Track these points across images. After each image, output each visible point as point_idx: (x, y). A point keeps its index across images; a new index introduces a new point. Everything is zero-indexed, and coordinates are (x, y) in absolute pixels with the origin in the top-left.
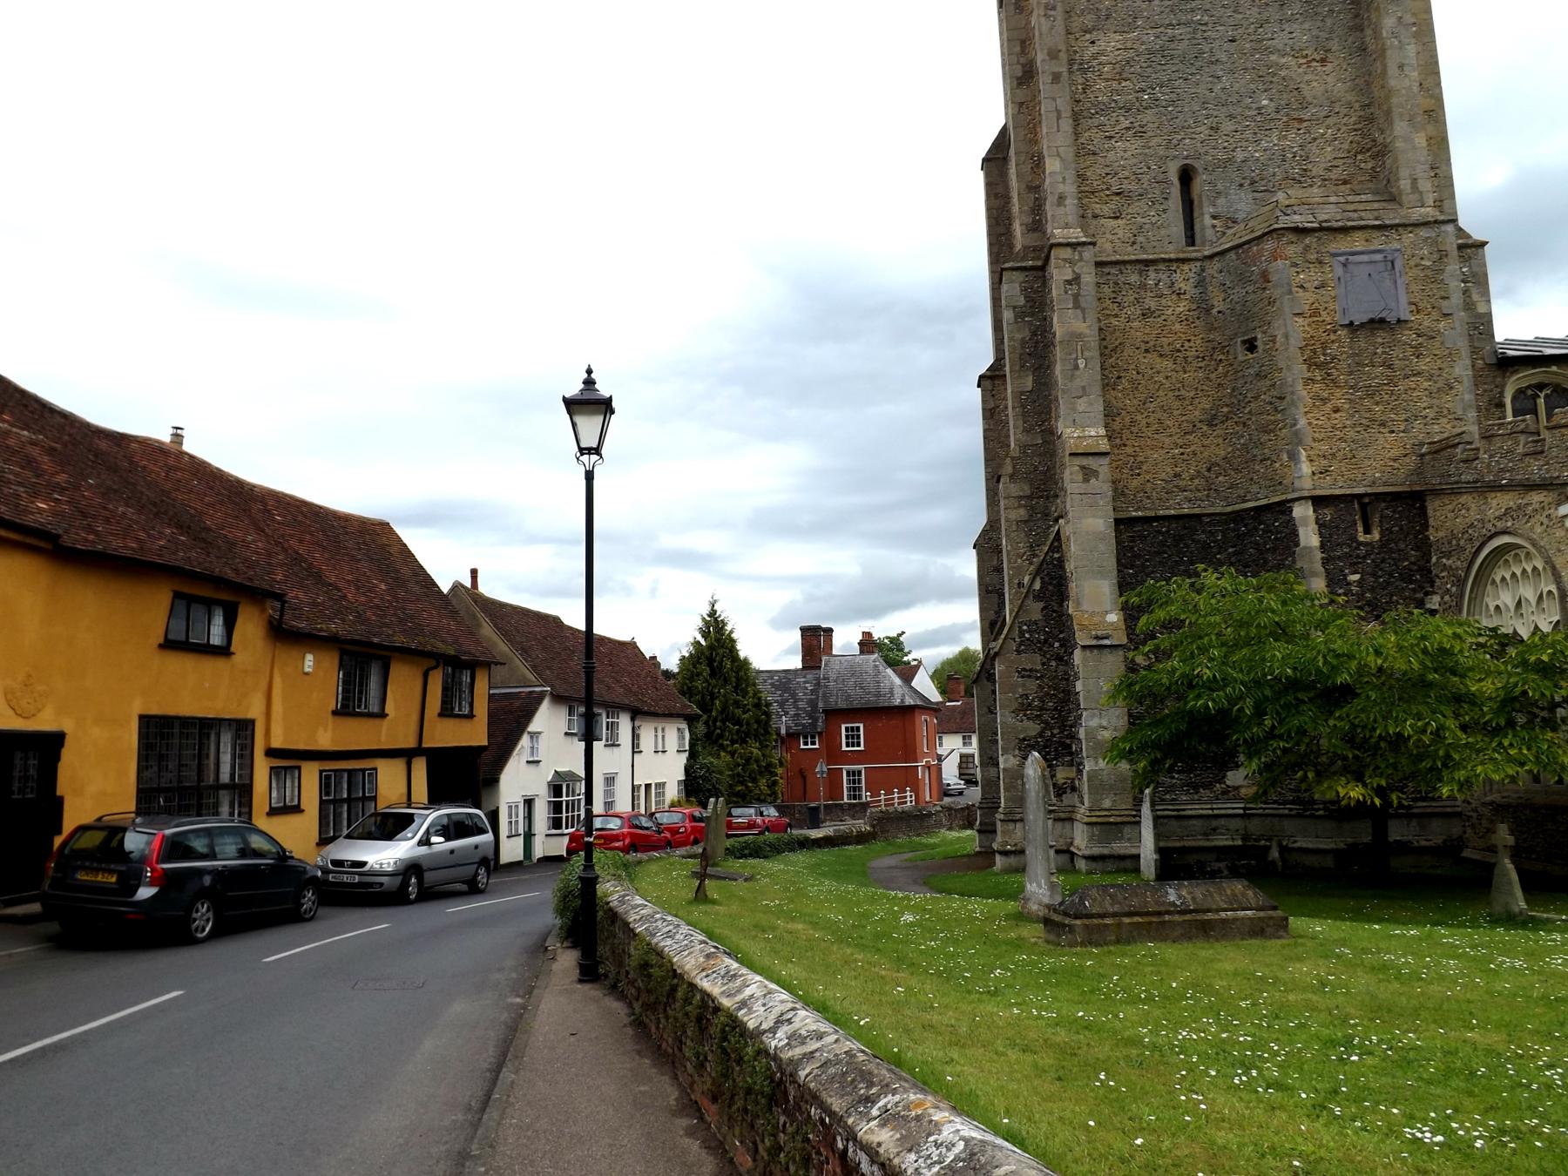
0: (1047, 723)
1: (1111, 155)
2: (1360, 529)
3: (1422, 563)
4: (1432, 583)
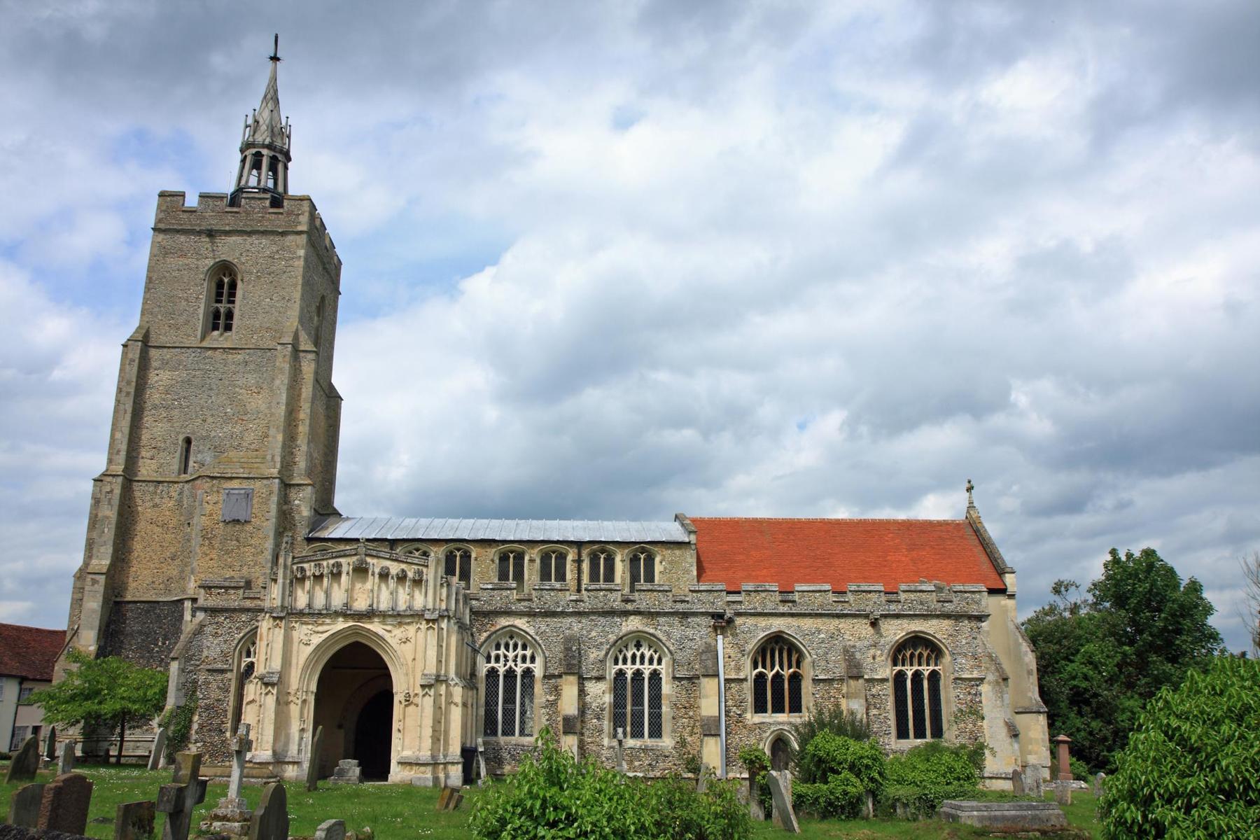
1: (155, 430)
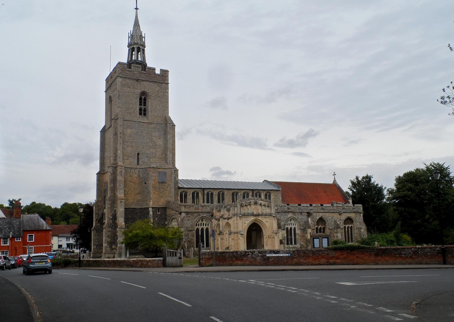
0: (111, 239)
2: (158, 212)
4: (166, 220)
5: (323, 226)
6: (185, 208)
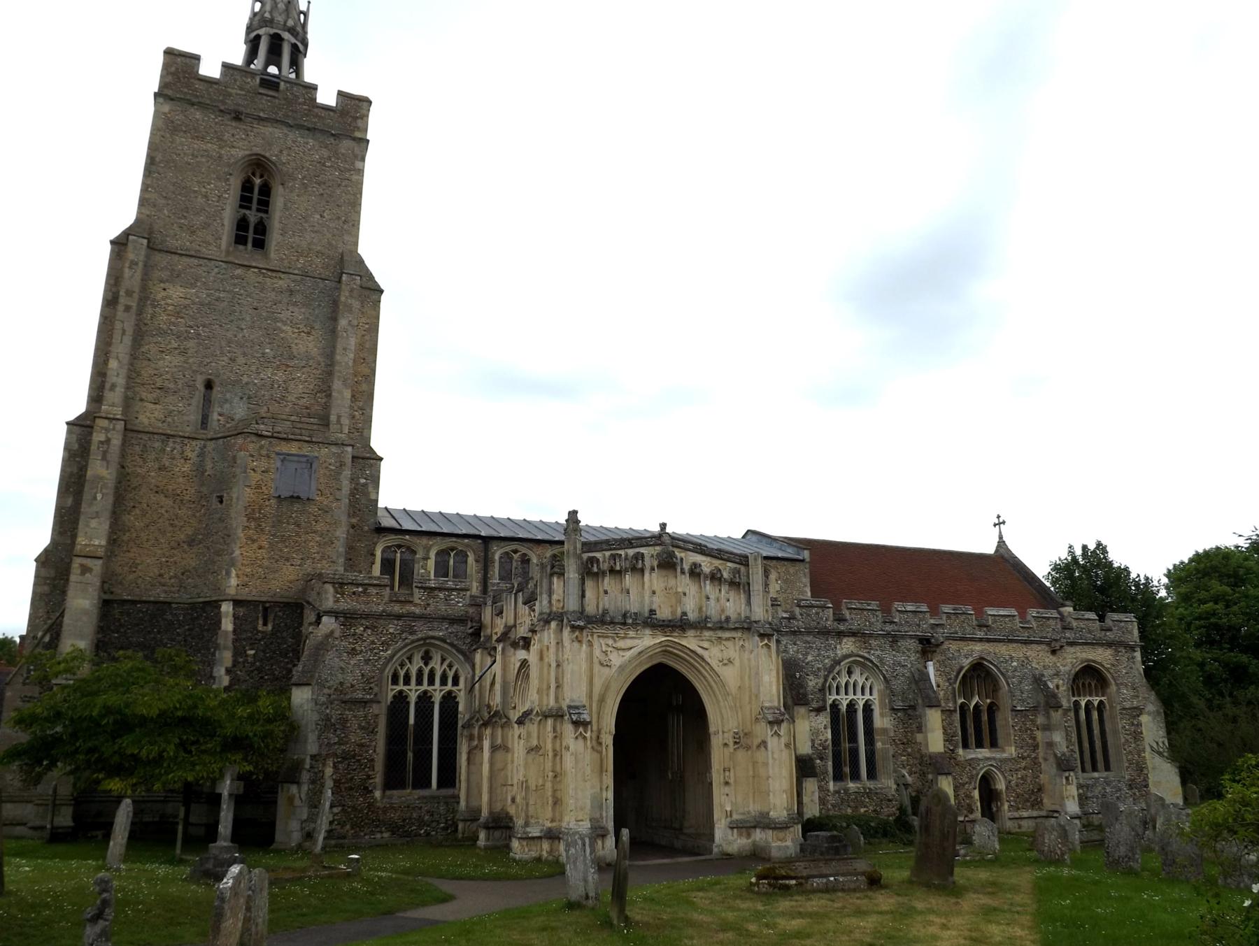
2: (261, 622)
3: (295, 646)
5: (988, 701)
6: (337, 593)
